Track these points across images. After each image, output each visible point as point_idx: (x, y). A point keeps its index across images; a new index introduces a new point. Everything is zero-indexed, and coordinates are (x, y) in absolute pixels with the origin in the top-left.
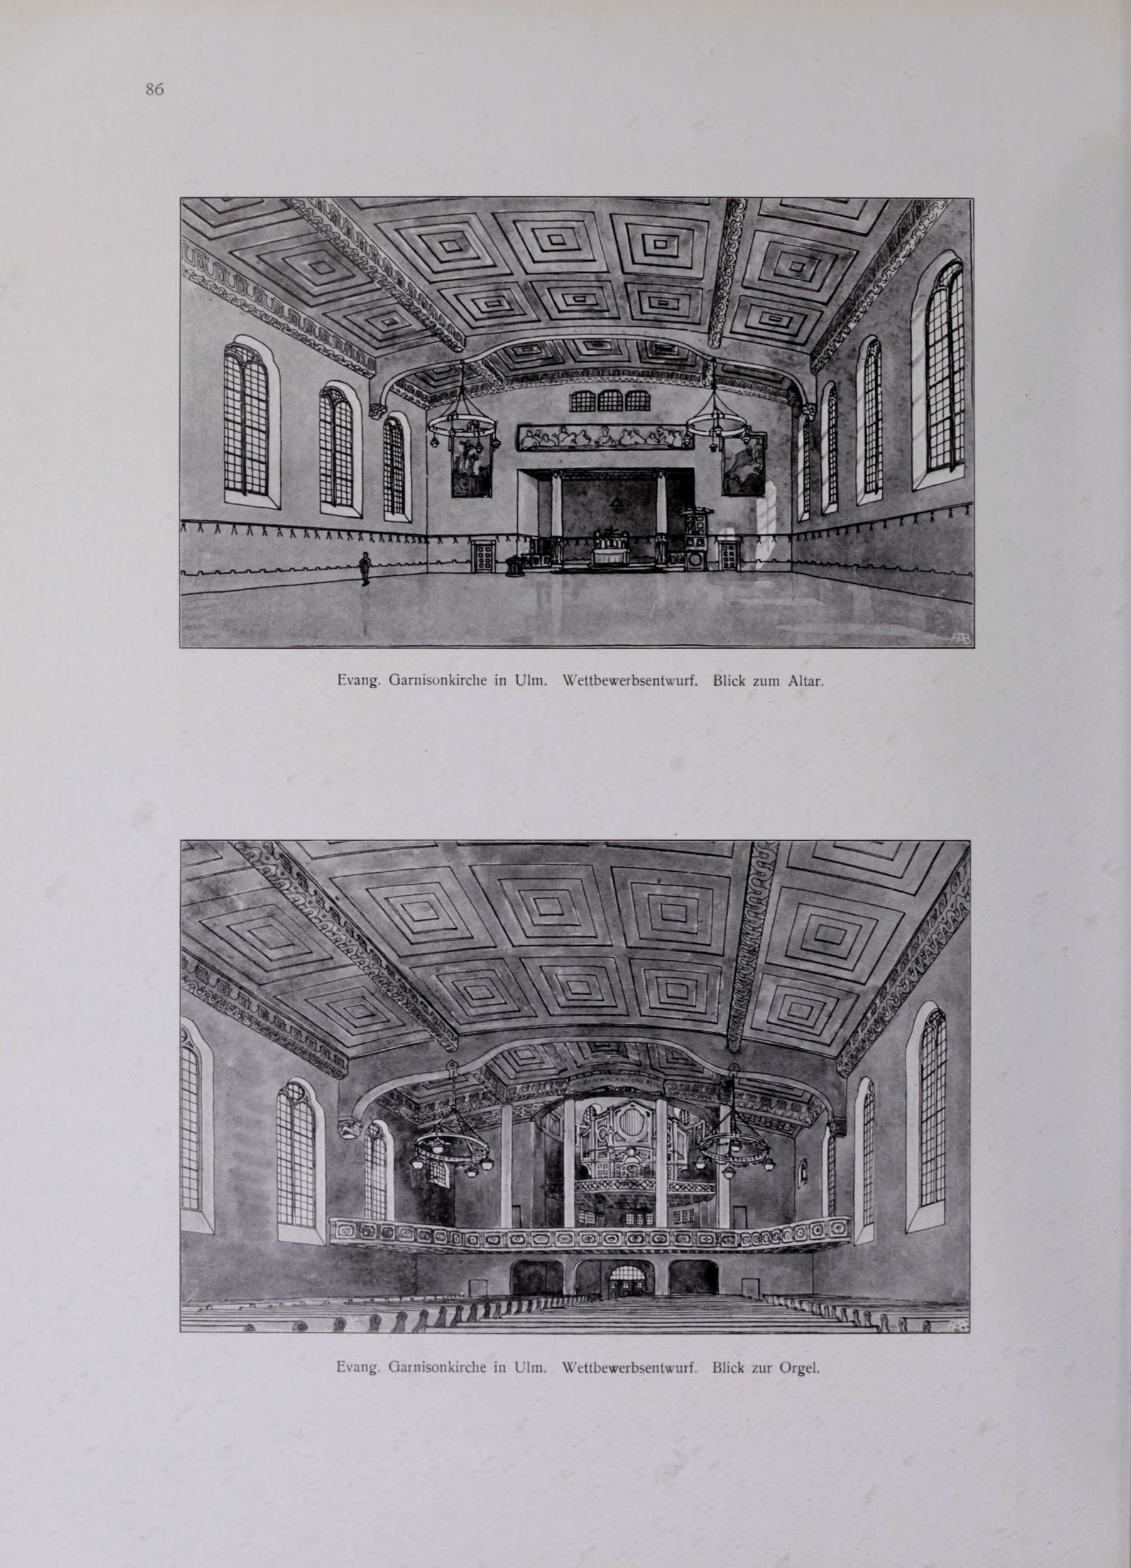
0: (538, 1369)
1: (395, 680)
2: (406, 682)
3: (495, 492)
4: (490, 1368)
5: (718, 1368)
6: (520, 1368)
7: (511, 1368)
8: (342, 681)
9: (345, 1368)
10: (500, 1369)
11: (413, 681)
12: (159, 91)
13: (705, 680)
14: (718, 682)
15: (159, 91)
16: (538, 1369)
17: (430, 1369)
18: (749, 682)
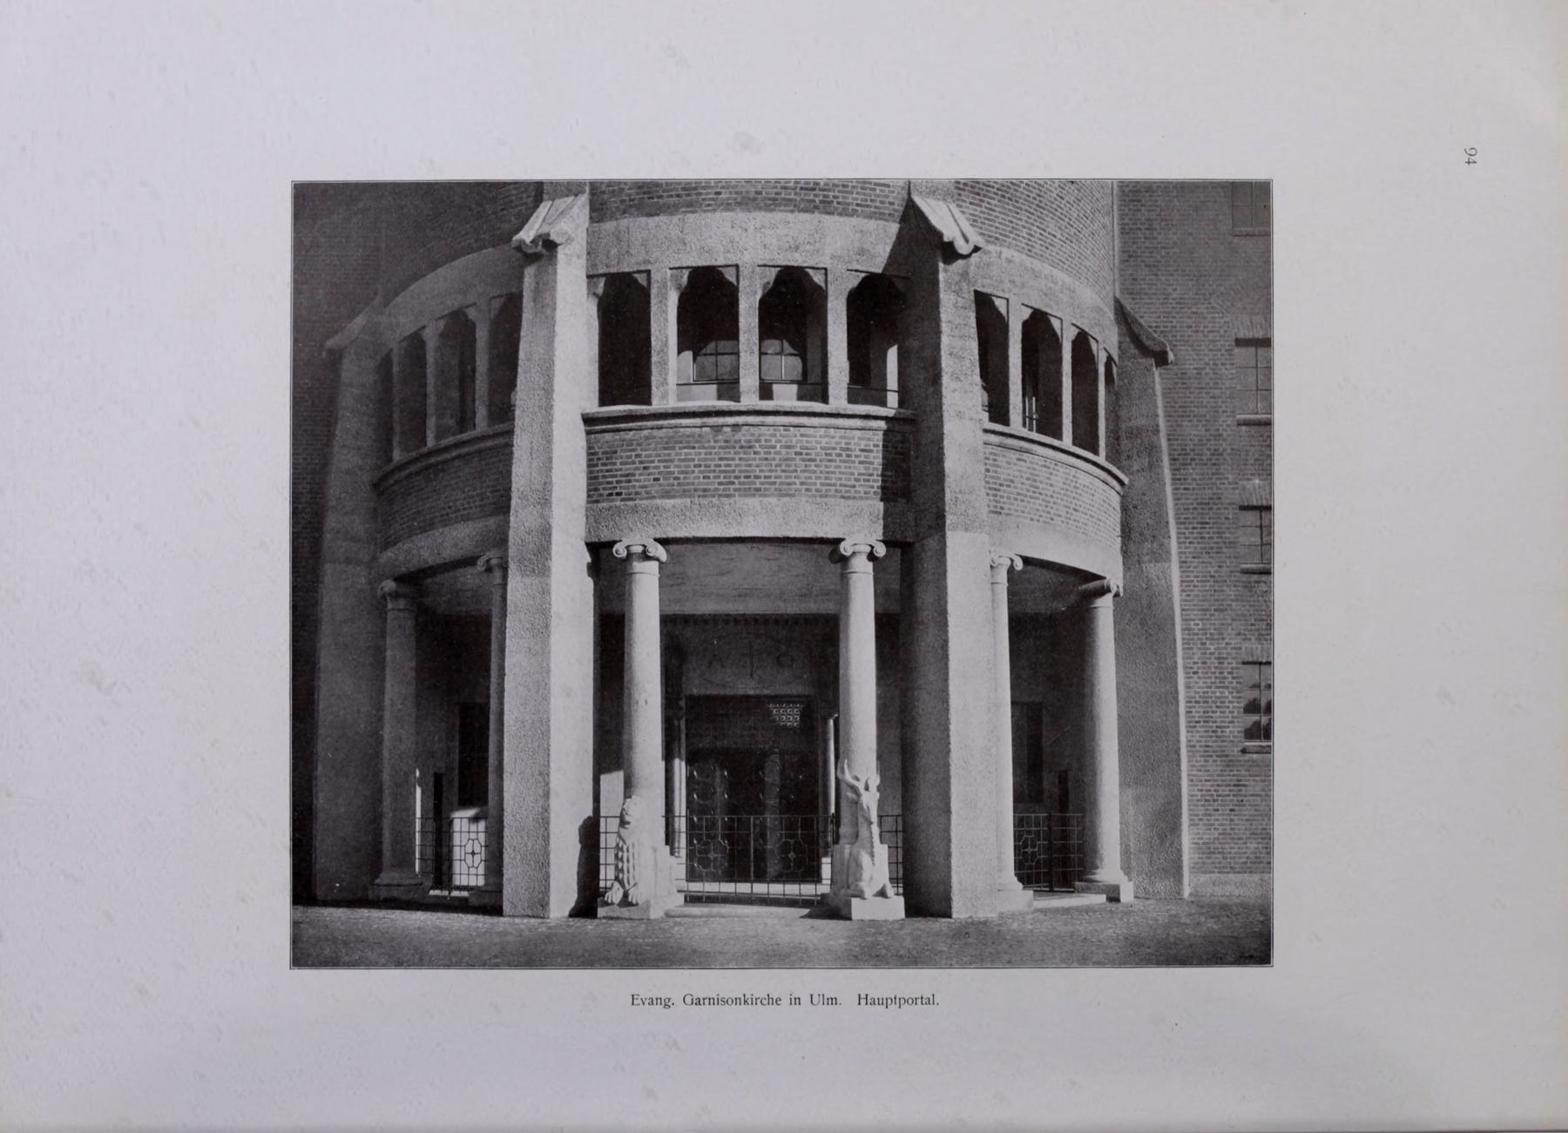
0: (833, 1001)
4: (785, 1001)
7: (805, 1000)
16: (833, 1001)
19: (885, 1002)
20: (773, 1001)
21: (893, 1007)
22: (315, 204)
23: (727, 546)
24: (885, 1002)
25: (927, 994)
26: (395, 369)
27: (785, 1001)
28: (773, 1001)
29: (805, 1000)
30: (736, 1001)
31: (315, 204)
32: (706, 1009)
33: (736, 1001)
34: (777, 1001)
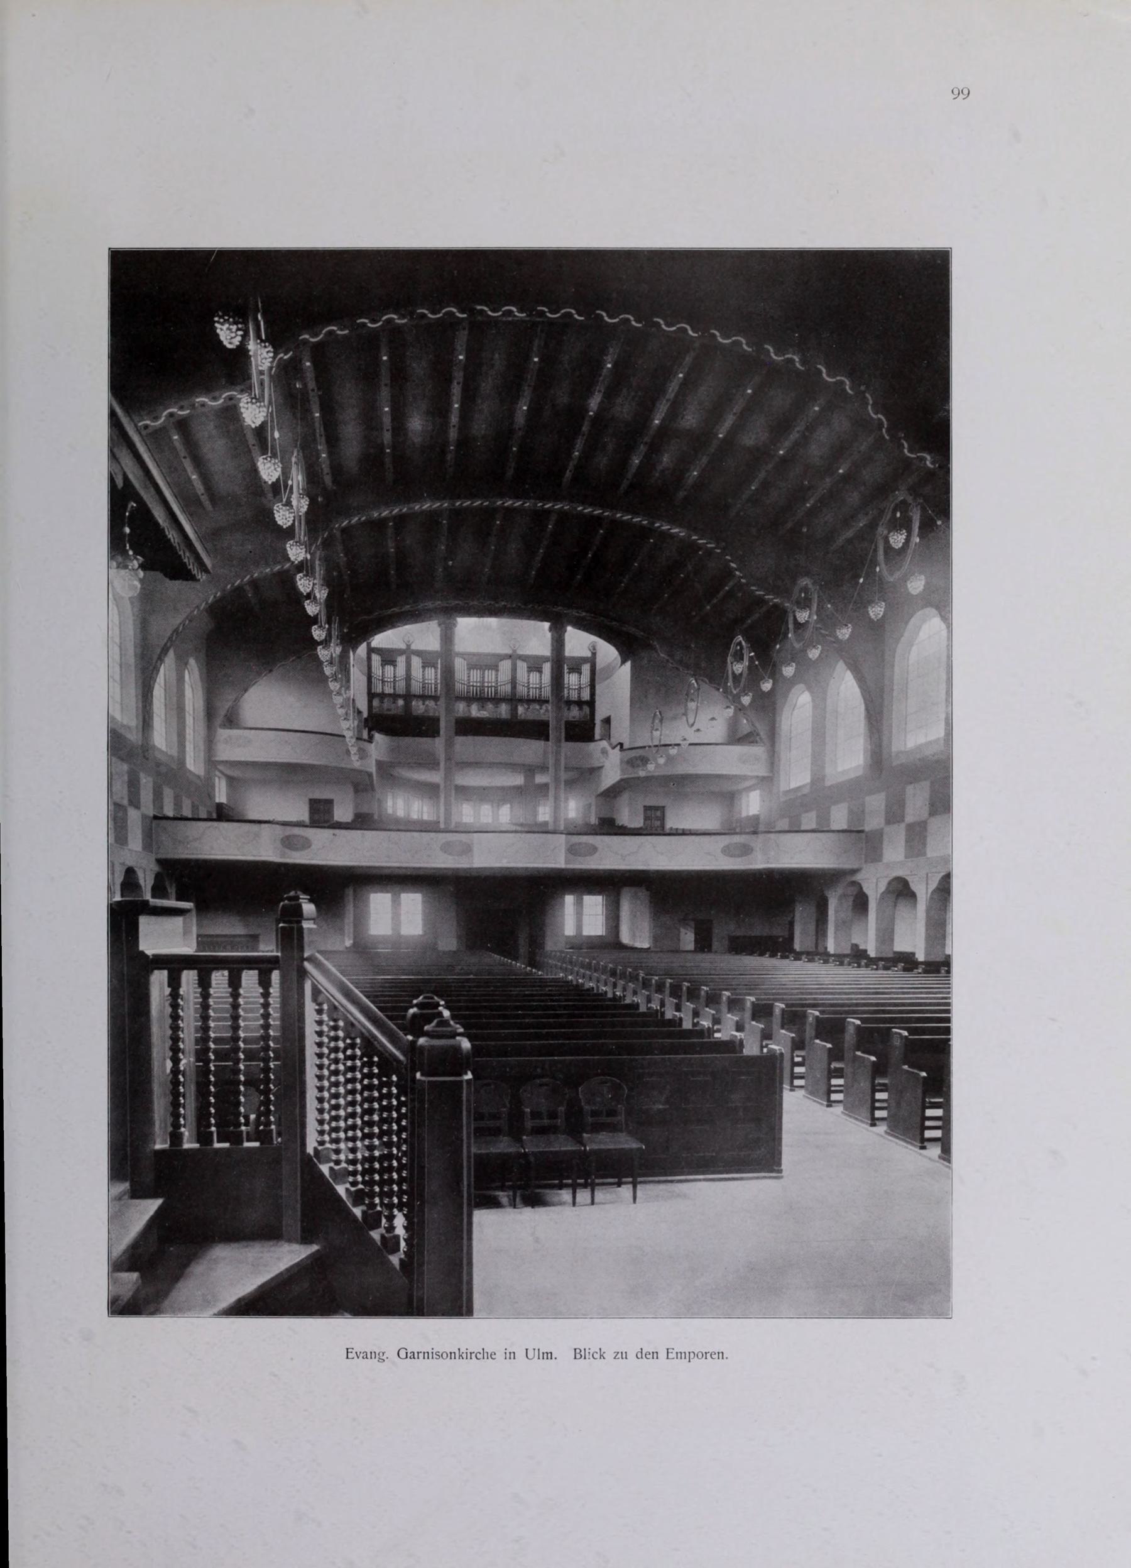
0: (549, 1355)
2: (413, 1356)
3: (955, 1313)
4: (500, 1356)
5: (579, 1354)
6: (530, 1355)
7: (520, 1354)
8: (350, 1355)
9: (354, 1355)
10: (512, 1355)
11: (421, 1355)
12: (956, 92)
13: (564, 1354)
14: (578, 1356)
15: (956, 92)
16: (549, 1355)
17: (440, 1356)
18: (609, 1355)
19: (687, 1356)
20: (377, 1356)
21: (695, 1361)
22: (942, 1311)
23: (265, 726)
24: (687, 1356)
25: (489, 1350)
26: (449, 457)
27: (500, 1356)
28: (377, 1356)
29: (520, 1354)
30: (451, 1355)
31: (942, 1311)
32: (420, 1363)
33: (451, 1355)
34: (492, 1356)
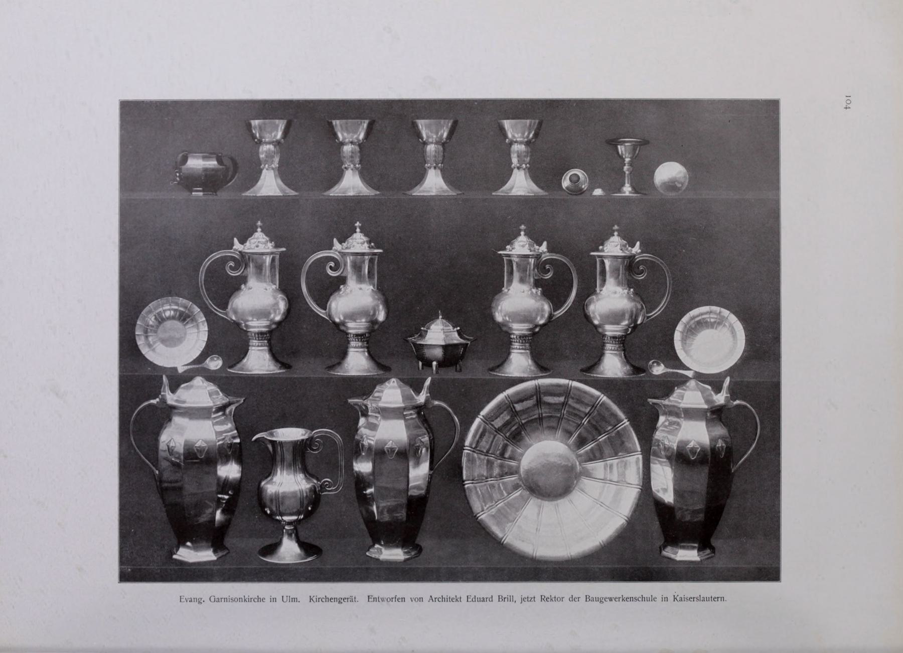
0: (295, 600)
1: (212, 599)
4: (268, 600)
7: (279, 599)
10: (274, 600)
16: (295, 600)
27: (268, 600)
30: (240, 600)
